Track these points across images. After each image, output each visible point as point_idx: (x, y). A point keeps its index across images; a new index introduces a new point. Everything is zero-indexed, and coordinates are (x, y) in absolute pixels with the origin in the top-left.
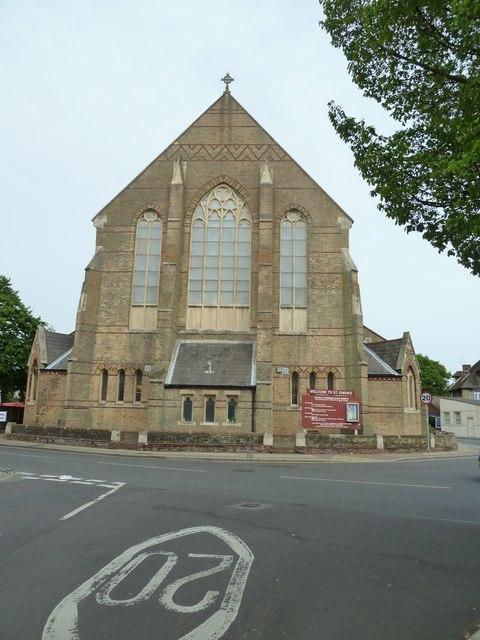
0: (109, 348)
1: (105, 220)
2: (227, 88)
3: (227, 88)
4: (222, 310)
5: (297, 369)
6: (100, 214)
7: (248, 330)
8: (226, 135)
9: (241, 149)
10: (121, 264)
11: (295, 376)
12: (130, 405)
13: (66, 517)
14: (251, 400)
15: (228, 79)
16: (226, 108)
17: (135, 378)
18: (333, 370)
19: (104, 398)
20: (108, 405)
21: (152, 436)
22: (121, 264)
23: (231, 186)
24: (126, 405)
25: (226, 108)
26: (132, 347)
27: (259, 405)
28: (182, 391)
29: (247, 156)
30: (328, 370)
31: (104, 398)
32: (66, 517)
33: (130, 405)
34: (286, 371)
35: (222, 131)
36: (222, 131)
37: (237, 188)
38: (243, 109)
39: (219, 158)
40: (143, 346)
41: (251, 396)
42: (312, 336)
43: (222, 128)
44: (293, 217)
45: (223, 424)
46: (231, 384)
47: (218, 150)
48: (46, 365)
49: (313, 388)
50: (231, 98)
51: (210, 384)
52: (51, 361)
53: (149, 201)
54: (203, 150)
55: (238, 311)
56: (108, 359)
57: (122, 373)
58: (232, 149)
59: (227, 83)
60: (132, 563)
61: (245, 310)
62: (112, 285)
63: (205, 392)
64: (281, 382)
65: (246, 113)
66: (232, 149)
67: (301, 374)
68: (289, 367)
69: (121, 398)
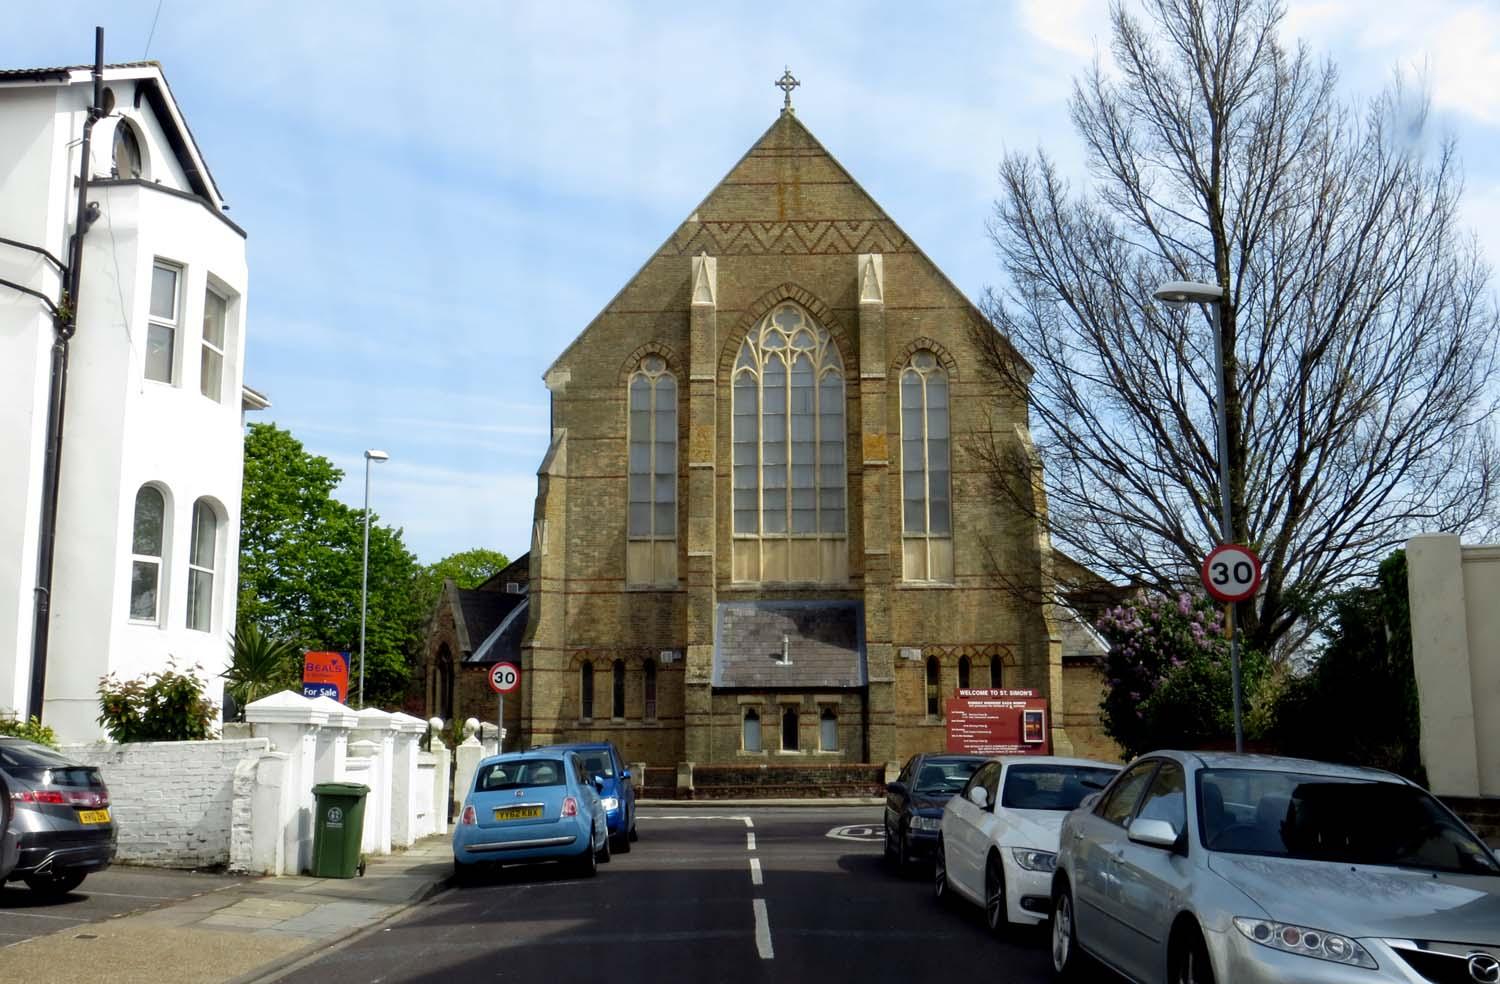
0: (593, 621)
1: (566, 377)
2: (787, 101)
3: (787, 101)
4: (796, 544)
5: (936, 652)
6: (558, 365)
7: (844, 582)
8: (789, 201)
9: (822, 226)
10: (603, 462)
11: (933, 667)
12: (636, 724)
13: (1191, 957)
14: (859, 709)
15: (787, 83)
16: (788, 141)
17: (644, 675)
18: (1002, 652)
19: (588, 712)
20: (597, 725)
21: (700, 776)
22: (603, 462)
23: (803, 306)
24: (629, 725)
25: (788, 141)
26: (635, 620)
27: (873, 718)
28: (742, 699)
29: (832, 245)
30: (991, 652)
31: (588, 712)
32: (1191, 957)
33: (636, 724)
34: (916, 654)
35: (781, 192)
36: (781, 192)
37: (815, 308)
38: (820, 147)
39: (778, 248)
40: (655, 612)
41: (859, 702)
42: (963, 590)
43: (781, 187)
44: (921, 371)
45: (815, 753)
46: (825, 683)
47: (776, 231)
48: (469, 654)
49: (965, 685)
50: (797, 126)
51: (789, 684)
52: (476, 645)
53: (645, 339)
54: (747, 234)
55: (826, 547)
56: (593, 641)
57: (619, 668)
58: (803, 230)
59: (787, 91)
60: (296, 964)
61: (838, 543)
62: (589, 503)
63: (780, 699)
64: (908, 674)
65: (827, 155)
66: (803, 230)
67: (944, 661)
68: (922, 647)
69: (619, 711)
